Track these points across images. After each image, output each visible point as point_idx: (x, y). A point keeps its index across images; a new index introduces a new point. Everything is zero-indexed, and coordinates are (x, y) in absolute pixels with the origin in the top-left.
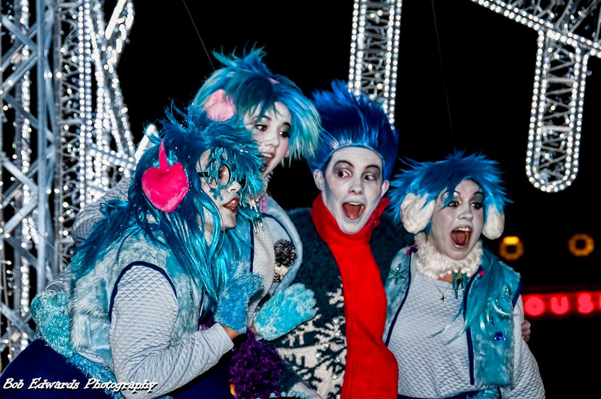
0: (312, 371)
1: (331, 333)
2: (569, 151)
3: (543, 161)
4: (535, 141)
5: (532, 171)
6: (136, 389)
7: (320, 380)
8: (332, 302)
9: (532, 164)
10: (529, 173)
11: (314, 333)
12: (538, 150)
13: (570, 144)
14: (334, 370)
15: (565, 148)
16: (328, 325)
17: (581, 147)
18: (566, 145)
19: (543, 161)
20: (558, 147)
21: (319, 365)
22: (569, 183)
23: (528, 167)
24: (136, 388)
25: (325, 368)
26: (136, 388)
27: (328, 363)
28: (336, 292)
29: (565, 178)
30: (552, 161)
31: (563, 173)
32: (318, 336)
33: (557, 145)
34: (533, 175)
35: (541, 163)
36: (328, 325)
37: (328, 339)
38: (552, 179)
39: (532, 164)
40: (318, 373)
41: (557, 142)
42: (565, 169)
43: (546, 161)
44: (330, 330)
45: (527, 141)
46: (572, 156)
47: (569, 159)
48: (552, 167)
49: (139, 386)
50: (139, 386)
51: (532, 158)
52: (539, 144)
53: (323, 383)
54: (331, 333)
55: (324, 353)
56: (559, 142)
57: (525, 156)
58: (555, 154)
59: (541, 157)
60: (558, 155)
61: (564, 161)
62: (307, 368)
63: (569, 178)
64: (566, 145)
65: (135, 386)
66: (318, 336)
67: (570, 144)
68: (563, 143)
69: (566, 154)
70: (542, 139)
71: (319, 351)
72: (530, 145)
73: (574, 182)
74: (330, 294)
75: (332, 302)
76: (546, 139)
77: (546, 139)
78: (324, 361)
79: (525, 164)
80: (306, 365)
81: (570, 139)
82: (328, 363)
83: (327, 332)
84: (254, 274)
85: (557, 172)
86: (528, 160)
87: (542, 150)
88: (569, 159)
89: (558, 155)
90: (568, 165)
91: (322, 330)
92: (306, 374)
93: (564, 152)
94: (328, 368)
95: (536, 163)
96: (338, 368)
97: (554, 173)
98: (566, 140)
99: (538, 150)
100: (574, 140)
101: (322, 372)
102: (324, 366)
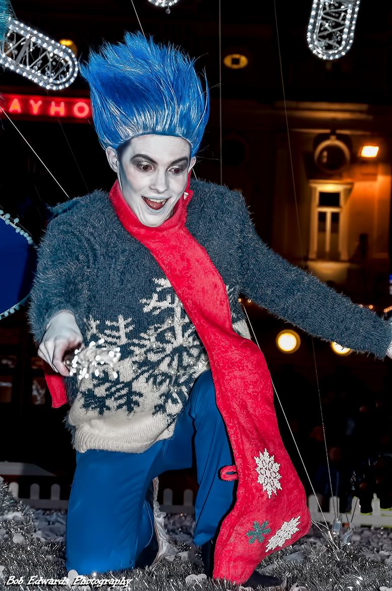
0: (129, 385)
1: (146, 343)
2: (347, 23)
3: (322, 29)
4: (318, 9)
5: (312, 38)
6: (116, 585)
7: (141, 395)
8: (146, 309)
9: (313, 32)
10: (309, 40)
11: (128, 345)
12: (319, 18)
13: (349, 16)
14: (154, 383)
15: (344, 19)
16: (142, 335)
17: (358, 20)
18: (345, 16)
19: (322, 29)
20: (338, 18)
21: (137, 377)
22: (343, 53)
23: (309, 34)
24: (115, 584)
25: (145, 380)
26: (115, 584)
27: (146, 375)
28: (151, 298)
29: (341, 48)
30: (330, 30)
31: (339, 43)
32: (132, 348)
33: (337, 15)
34: (312, 42)
35: (320, 31)
36: (142, 335)
37: (143, 350)
38: (329, 47)
39: (313, 32)
40: (136, 386)
41: (335, 13)
42: (342, 39)
43: (326, 30)
44: (145, 339)
45: (310, 9)
46: (350, 28)
47: (346, 30)
48: (330, 36)
49: (117, 582)
50: (117, 582)
51: (314, 25)
52: (321, 12)
53: (143, 398)
54: (146, 343)
55: (141, 365)
56: (340, 13)
57: (307, 23)
58: (334, 24)
59: (321, 25)
60: (337, 25)
61: (342, 31)
62: (123, 382)
63: (345, 48)
64: (345, 16)
65: (114, 582)
66: (132, 348)
67: (349, 16)
68: (343, 14)
69: (344, 25)
70: (324, 9)
71: (134, 363)
72: (313, 13)
73: (348, 53)
74: (144, 301)
75: (146, 309)
76: (328, 8)
77: (328, 8)
78: (142, 373)
79: (306, 31)
80: (121, 380)
81: (350, 11)
82: (146, 375)
83: (143, 342)
84: (79, 339)
85: (334, 42)
86: (310, 27)
87: (323, 19)
88: (346, 30)
89: (337, 25)
90: (345, 36)
91: (136, 341)
92: (123, 388)
93: (342, 22)
94: (147, 380)
95: (317, 31)
96: (159, 379)
97: (331, 42)
98: (346, 12)
99: (319, 18)
100: (353, 13)
101: (140, 385)
102: (142, 379)
